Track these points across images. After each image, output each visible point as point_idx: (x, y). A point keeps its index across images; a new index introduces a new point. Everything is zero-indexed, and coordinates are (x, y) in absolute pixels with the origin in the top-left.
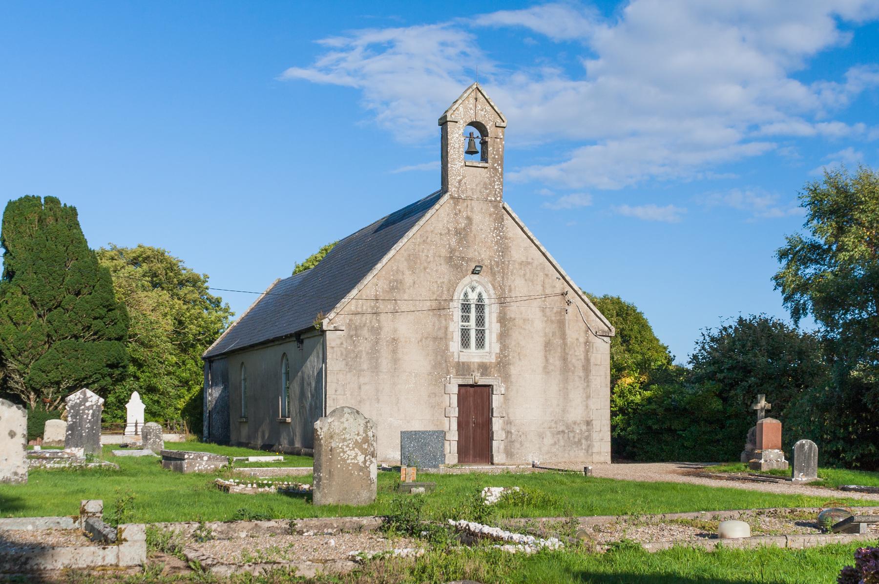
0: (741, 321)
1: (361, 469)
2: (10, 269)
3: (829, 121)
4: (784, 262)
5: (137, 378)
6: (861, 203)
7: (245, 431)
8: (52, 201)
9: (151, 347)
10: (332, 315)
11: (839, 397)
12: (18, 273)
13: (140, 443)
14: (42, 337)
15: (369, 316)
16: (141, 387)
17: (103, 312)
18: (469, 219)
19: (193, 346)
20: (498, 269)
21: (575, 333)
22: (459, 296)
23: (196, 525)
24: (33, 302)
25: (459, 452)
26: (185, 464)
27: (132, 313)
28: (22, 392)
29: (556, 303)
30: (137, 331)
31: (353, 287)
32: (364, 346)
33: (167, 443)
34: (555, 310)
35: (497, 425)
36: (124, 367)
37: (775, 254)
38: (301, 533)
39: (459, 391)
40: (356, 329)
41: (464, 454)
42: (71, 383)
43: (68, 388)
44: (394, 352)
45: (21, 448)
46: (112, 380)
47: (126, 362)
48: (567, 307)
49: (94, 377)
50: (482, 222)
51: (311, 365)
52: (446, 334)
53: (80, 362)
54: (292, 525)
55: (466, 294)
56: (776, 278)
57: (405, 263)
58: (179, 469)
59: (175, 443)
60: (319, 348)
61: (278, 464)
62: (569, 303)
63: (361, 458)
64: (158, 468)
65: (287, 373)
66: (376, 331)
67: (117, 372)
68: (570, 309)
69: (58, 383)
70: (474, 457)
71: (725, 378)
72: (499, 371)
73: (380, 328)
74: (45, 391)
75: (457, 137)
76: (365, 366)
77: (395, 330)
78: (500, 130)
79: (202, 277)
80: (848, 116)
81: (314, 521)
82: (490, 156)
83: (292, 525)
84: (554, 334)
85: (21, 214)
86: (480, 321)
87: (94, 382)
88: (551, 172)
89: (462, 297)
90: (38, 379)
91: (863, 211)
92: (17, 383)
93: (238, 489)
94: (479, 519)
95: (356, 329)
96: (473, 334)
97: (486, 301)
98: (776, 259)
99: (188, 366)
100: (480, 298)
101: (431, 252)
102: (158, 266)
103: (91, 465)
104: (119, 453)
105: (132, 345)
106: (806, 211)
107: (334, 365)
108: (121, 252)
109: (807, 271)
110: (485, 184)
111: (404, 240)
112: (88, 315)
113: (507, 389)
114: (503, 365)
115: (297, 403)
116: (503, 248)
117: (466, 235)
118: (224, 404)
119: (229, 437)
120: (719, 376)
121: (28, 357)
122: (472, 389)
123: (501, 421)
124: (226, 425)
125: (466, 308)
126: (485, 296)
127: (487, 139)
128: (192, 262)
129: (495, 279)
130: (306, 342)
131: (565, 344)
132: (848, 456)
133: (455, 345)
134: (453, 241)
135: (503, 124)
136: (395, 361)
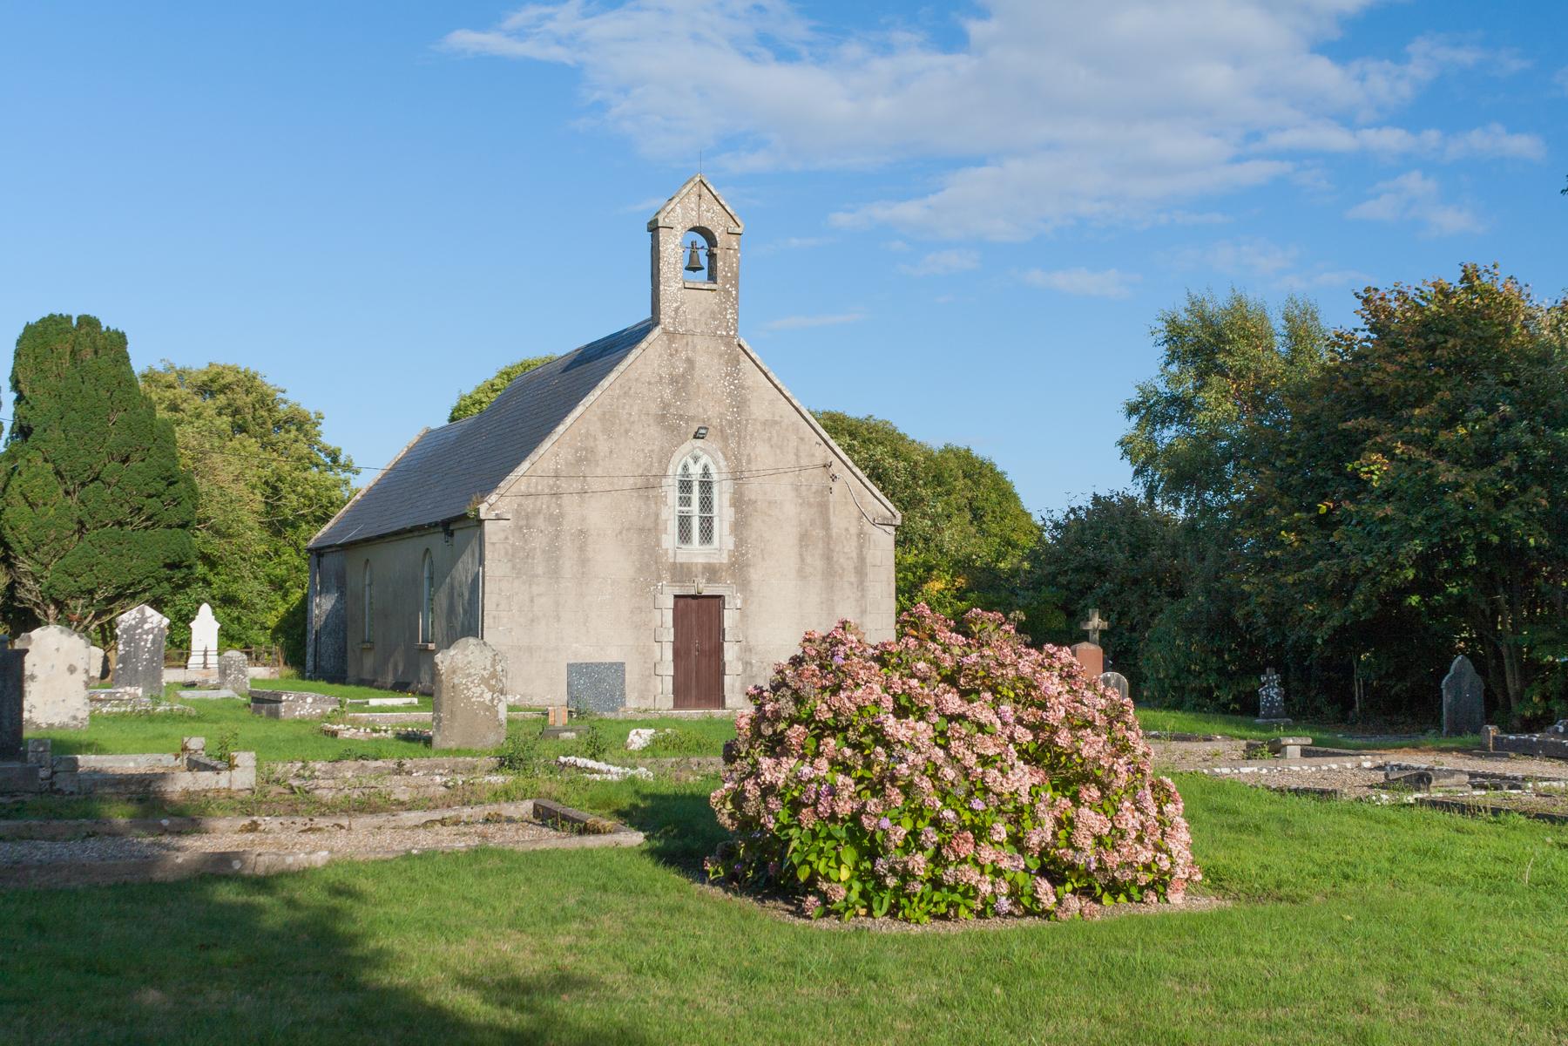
0: (1096, 498)
1: (488, 709)
2: (24, 423)
3: (1378, 125)
4: (1135, 419)
5: (208, 584)
6: (1229, 342)
7: (369, 661)
8: (88, 322)
9: (230, 536)
10: (493, 498)
11: (1209, 612)
12: (37, 430)
13: (214, 679)
14: (70, 525)
15: (546, 499)
16: (213, 597)
17: (161, 486)
18: (690, 361)
19: (294, 526)
20: (731, 430)
21: (843, 521)
22: (675, 469)
23: (300, 765)
24: (58, 473)
25: (676, 691)
26: (282, 708)
27: (203, 486)
28: (37, 605)
29: (818, 478)
30: (210, 513)
31: (518, 462)
32: (539, 542)
33: (253, 680)
34: (814, 488)
35: (730, 653)
36: (189, 567)
37: (1123, 409)
38: (409, 773)
39: (676, 604)
40: (527, 517)
41: (681, 695)
42: (111, 592)
43: (106, 599)
44: (582, 549)
45: (81, 686)
46: (174, 584)
47: (193, 559)
48: (831, 484)
49: (145, 583)
50: (709, 367)
51: (463, 569)
52: (656, 523)
53: (125, 561)
54: (400, 765)
55: (685, 467)
56: (1121, 443)
57: (598, 424)
58: (275, 714)
59: (263, 681)
60: (475, 542)
61: (409, 708)
62: (834, 478)
63: (488, 696)
64: (246, 712)
65: (431, 578)
66: (556, 520)
67: (178, 575)
68: (836, 486)
69: (91, 592)
70: (698, 699)
71: (1070, 582)
72: (733, 576)
73: (561, 515)
74: (72, 603)
75: (673, 248)
76: (540, 570)
77: (583, 519)
78: (733, 238)
79: (313, 416)
80: (1410, 118)
81: (425, 762)
82: (720, 274)
83: (400, 765)
84: (813, 522)
85: (46, 344)
86: (706, 504)
87: (144, 591)
88: (910, 211)
89: (680, 470)
90: (62, 587)
91: (1230, 353)
92: (30, 591)
93: (347, 735)
94: (593, 756)
95: (527, 517)
96: (696, 524)
97: (715, 477)
98: (1123, 415)
99: (285, 557)
100: (706, 472)
101: (636, 408)
102: (242, 400)
103: (160, 709)
104: (187, 694)
105: (203, 534)
106: (1163, 351)
107: (496, 569)
108: (181, 374)
109: (1166, 433)
110: (713, 312)
111: (597, 392)
112: (140, 493)
113: (745, 601)
114: (738, 567)
115: (444, 623)
116: (739, 401)
117: (686, 383)
118: (340, 623)
119: (345, 672)
120: (1062, 580)
121: (48, 553)
122: (694, 602)
123: (736, 647)
124: (342, 653)
125: (685, 486)
126: (713, 470)
127: (716, 251)
128: (295, 389)
129: (727, 446)
130: (457, 533)
131: (829, 536)
132: (1223, 695)
133: (670, 538)
134: (668, 393)
135: (738, 230)
136: (583, 562)
